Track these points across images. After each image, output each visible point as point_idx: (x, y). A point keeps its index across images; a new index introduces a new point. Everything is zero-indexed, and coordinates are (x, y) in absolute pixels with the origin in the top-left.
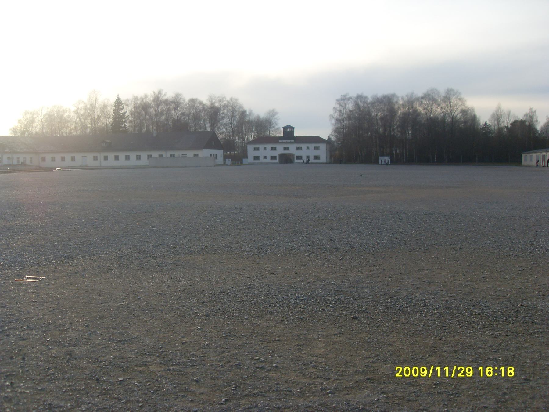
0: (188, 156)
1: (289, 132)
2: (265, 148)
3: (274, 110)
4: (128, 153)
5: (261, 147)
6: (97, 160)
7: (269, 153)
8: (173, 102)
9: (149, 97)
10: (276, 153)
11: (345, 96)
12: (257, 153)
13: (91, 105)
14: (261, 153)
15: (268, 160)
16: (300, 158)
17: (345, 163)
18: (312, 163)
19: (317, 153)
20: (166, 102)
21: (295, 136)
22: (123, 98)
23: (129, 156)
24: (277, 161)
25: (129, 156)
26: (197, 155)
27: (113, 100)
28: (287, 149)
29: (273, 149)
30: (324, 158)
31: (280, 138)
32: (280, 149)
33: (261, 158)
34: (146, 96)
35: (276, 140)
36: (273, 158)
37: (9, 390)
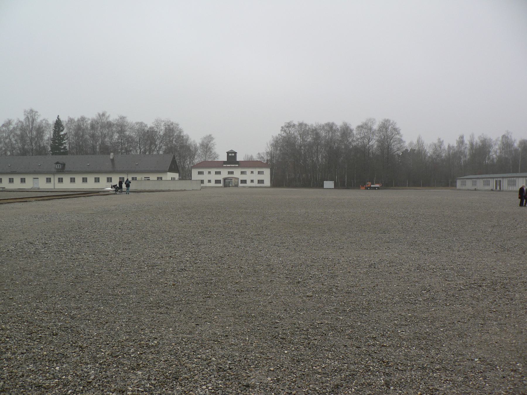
0: (151, 179)
1: (232, 158)
2: (209, 173)
3: (210, 135)
4: (209, 170)
5: (206, 171)
6: (50, 181)
7: (214, 177)
8: (118, 125)
9: (14, 123)
10: (220, 177)
11: (289, 123)
12: (201, 177)
13: (39, 126)
14: (205, 177)
15: (213, 184)
16: (244, 182)
17: (348, 188)
18: (506, 191)
19: (261, 177)
20: (110, 125)
21: (226, 160)
22: (64, 119)
23: (13, 179)
24: (221, 185)
25: (86, 178)
26: (161, 178)
27: (52, 121)
28: (232, 173)
29: (217, 173)
30: (267, 183)
31: (224, 163)
32: (224, 173)
33: (206, 182)
34: (83, 119)
35: (221, 165)
36: (218, 182)
37: (69, 392)
